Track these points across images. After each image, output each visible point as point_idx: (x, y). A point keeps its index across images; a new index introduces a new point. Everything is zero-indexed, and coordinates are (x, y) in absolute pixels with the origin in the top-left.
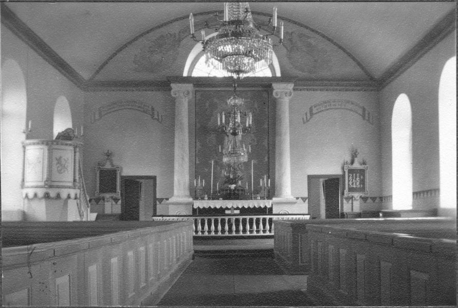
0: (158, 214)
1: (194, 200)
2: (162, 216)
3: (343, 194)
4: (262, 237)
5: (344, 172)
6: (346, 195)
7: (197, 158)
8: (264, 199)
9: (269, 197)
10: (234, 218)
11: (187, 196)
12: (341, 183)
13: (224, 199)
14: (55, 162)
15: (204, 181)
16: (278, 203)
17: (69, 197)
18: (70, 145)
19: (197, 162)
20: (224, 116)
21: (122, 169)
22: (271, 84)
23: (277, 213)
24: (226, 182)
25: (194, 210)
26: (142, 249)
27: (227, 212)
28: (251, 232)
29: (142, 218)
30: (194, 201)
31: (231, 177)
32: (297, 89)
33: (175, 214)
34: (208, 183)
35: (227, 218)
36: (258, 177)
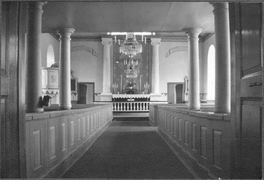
0: (95, 101)
1: (113, 94)
2: (98, 102)
3: (184, 92)
4: (144, 112)
5: (185, 82)
6: (186, 93)
7: (114, 74)
8: (146, 94)
9: (149, 93)
10: (131, 103)
11: (109, 92)
12: (183, 85)
13: (127, 94)
14: (50, 77)
15: (117, 85)
16: (153, 96)
17: (57, 93)
18: (57, 69)
19: (114, 76)
20: (126, 61)
21: (78, 79)
22: (150, 39)
23: (152, 100)
24: (128, 86)
25: (113, 99)
26: (97, 113)
27: (128, 100)
28: (139, 109)
29: (87, 103)
30: (113, 95)
31: (131, 83)
32: (163, 41)
33: (103, 101)
34: (119, 86)
35: (128, 103)
36: (143, 84)
